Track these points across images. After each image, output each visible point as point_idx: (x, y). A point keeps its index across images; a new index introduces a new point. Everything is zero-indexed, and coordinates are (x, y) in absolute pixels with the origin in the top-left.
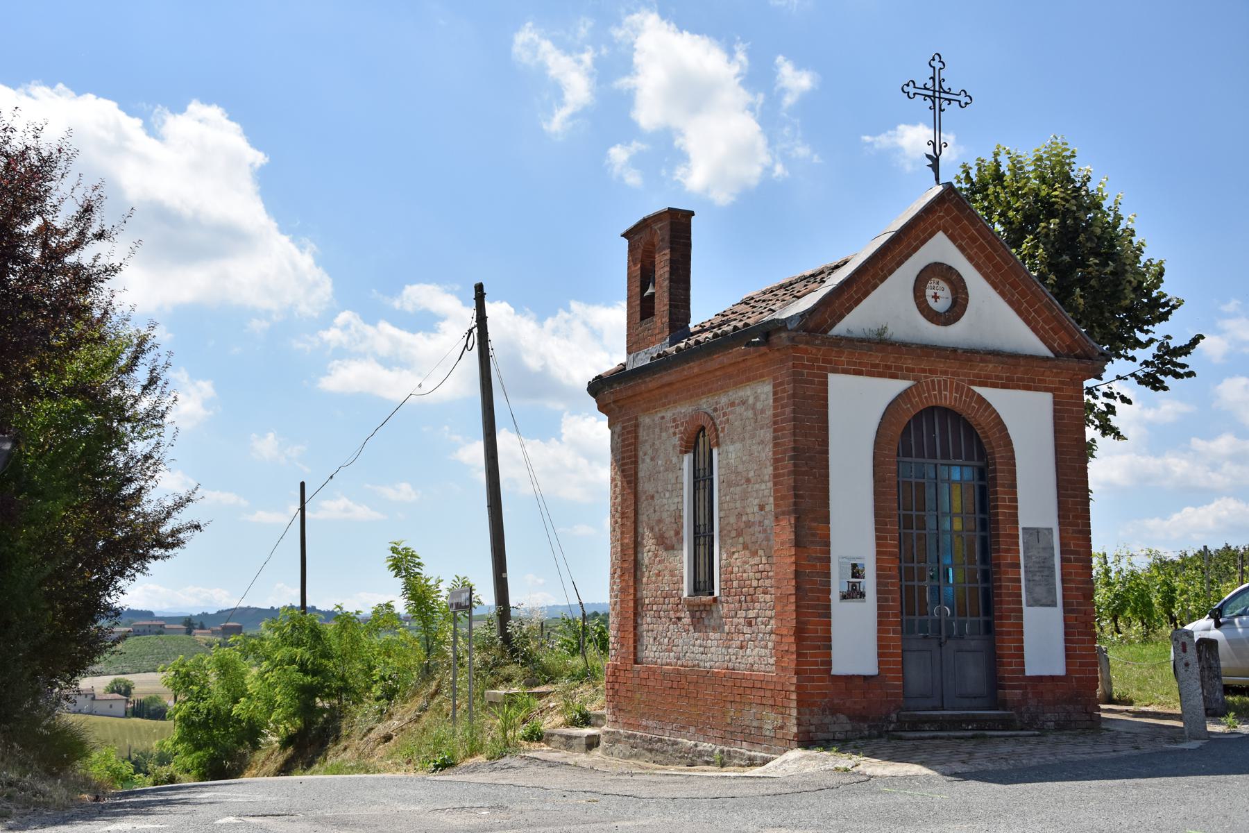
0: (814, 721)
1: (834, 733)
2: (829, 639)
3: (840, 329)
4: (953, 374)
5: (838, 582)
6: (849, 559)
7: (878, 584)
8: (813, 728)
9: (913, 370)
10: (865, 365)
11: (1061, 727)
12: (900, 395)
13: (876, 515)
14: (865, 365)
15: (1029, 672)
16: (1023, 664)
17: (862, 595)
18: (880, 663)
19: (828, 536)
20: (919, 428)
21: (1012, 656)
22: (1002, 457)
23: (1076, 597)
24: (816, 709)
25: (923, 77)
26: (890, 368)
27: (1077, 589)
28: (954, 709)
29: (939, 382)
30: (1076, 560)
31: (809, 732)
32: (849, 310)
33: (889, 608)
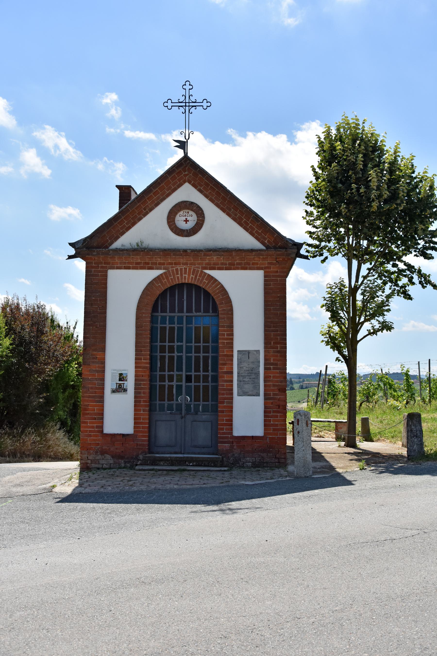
0: (91, 457)
1: (103, 464)
2: (102, 414)
3: (118, 244)
4: (191, 264)
5: (110, 383)
6: (118, 371)
7: (136, 384)
8: (89, 462)
9: (164, 264)
10: (132, 263)
11: (255, 465)
12: (155, 279)
13: (136, 346)
14: (132, 263)
15: (236, 433)
16: (232, 429)
17: (125, 390)
18: (135, 427)
19: (104, 359)
20: (172, 296)
21: (225, 425)
22: (223, 310)
23: (273, 390)
24: (92, 451)
25: (197, 96)
26: (148, 264)
27: (274, 386)
28: (188, 453)
29: (181, 270)
30: (274, 369)
31: (87, 463)
32: (123, 233)
33: (141, 397)
